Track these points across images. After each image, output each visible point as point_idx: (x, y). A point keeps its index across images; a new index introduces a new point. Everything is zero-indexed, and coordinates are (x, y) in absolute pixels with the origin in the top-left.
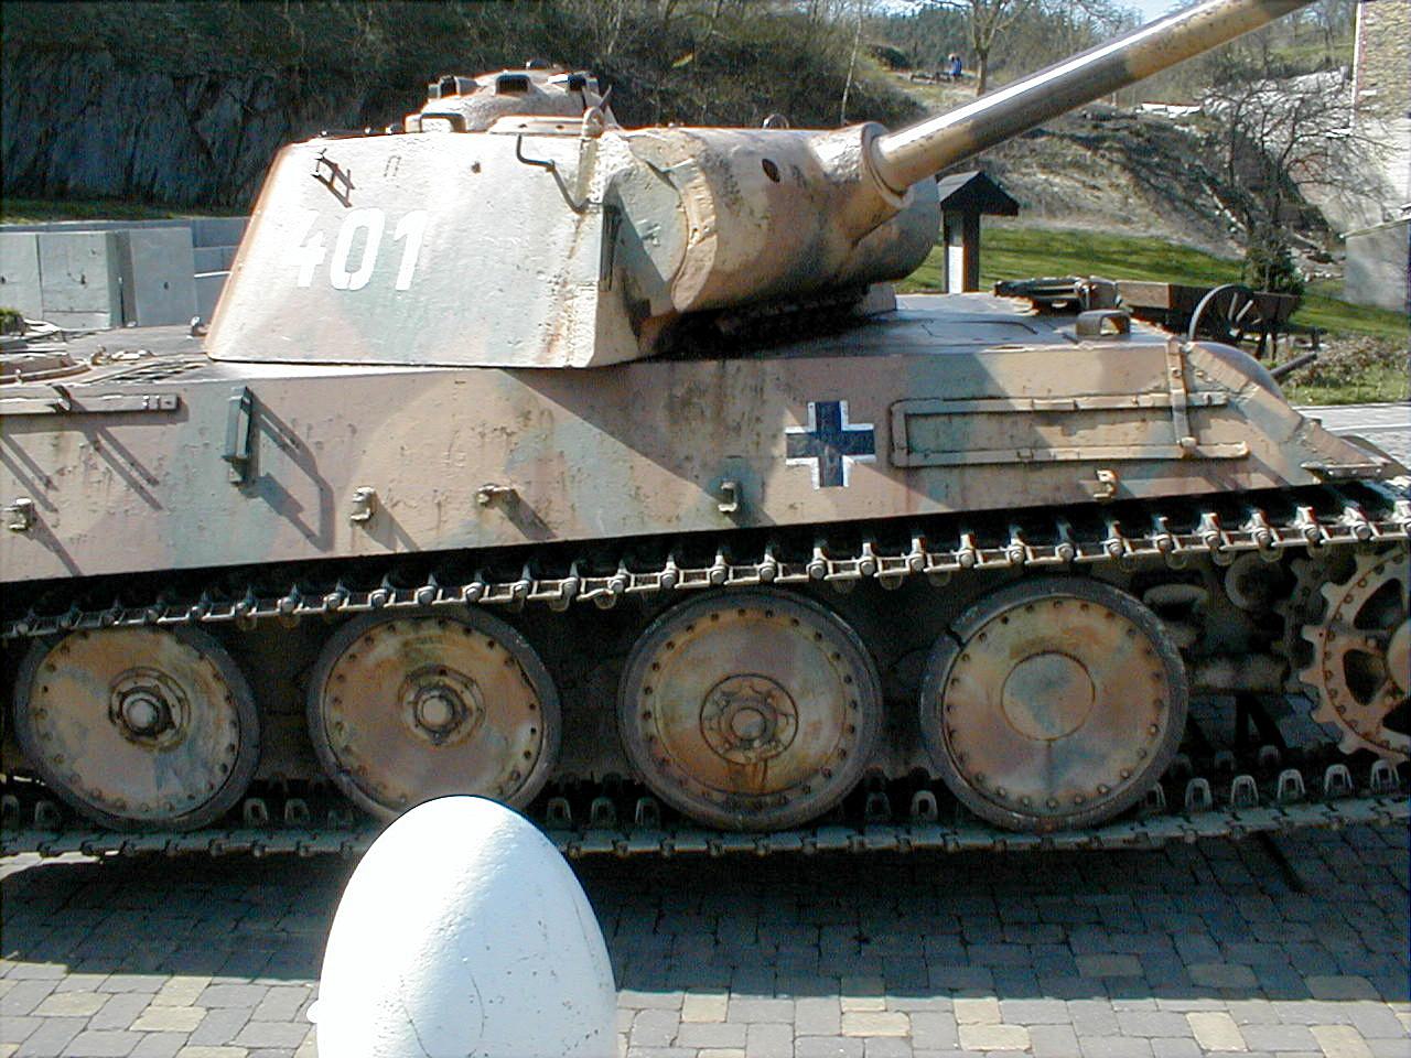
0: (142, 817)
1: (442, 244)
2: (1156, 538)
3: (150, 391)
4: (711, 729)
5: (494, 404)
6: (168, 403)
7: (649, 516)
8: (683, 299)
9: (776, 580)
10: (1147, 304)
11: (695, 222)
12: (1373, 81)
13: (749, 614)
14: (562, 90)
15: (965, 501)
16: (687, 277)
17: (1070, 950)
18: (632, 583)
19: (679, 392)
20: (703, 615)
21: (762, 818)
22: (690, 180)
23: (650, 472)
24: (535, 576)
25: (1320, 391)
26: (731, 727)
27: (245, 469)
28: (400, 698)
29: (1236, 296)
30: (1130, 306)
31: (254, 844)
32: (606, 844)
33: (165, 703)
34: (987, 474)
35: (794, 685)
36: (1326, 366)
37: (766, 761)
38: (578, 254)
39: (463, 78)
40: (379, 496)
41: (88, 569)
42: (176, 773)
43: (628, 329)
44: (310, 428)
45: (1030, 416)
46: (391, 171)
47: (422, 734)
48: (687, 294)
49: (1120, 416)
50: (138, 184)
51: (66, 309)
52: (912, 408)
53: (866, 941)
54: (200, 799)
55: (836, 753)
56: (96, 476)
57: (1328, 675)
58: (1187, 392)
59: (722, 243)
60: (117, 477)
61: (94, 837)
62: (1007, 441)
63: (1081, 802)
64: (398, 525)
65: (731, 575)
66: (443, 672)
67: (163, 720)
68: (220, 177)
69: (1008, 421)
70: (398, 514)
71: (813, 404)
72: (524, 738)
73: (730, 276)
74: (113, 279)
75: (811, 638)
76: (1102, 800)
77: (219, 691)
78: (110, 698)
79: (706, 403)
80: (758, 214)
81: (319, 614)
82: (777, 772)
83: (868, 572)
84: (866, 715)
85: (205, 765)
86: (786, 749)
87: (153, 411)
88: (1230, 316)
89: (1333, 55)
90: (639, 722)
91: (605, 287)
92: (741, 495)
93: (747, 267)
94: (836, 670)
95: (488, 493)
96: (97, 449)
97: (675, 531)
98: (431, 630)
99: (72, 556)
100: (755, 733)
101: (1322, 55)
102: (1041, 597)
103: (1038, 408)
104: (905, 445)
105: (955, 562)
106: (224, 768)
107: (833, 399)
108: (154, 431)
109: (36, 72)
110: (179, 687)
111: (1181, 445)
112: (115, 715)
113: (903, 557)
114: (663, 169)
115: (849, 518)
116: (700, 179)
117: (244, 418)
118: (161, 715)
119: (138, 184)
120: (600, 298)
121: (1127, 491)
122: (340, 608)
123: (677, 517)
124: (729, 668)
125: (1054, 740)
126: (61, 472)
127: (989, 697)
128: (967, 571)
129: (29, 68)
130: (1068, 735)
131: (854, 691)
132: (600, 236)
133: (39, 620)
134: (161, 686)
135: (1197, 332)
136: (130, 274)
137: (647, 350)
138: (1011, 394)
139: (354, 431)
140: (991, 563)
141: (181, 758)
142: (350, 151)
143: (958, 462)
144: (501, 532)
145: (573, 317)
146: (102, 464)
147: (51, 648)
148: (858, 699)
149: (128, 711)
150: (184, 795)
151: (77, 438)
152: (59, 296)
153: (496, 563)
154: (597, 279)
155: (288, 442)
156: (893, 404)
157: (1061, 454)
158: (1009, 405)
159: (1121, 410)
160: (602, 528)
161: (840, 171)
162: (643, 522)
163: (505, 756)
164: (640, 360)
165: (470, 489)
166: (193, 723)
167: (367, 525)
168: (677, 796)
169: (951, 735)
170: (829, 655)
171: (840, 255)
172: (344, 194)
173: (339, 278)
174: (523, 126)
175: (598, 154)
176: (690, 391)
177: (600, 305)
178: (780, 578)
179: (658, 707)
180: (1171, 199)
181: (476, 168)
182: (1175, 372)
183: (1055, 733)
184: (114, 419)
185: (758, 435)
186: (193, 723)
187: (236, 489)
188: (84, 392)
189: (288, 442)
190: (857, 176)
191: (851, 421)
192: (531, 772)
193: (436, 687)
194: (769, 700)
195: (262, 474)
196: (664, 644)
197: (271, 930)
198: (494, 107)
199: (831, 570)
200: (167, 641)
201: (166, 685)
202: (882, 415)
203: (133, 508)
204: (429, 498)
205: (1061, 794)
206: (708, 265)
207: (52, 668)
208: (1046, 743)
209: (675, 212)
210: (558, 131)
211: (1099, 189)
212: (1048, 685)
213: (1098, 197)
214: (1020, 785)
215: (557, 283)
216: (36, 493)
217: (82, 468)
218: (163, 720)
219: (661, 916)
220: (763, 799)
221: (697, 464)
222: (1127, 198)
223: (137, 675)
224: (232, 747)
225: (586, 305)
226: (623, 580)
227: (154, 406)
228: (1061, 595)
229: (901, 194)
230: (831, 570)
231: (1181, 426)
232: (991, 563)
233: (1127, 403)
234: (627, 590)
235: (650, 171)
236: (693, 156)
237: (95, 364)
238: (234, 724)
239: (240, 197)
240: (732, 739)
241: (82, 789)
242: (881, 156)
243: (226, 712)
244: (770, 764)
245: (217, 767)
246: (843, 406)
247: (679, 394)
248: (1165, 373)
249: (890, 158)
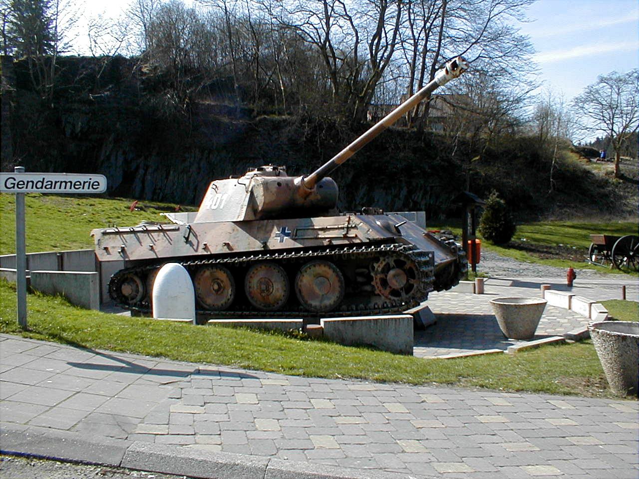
5: (229, 227)
14: (272, 170)
27: (187, 239)
35: (273, 281)
43: (253, 213)
47: (214, 292)
57: (377, 283)
70: (210, 247)
79: (264, 228)
92: (265, 245)
109: (238, 166)
116: (262, 186)
117: (188, 230)
124: (261, 277)
129: (236, 166)
146: (165, 239)
165: (222, 243)
233: (336, 227)
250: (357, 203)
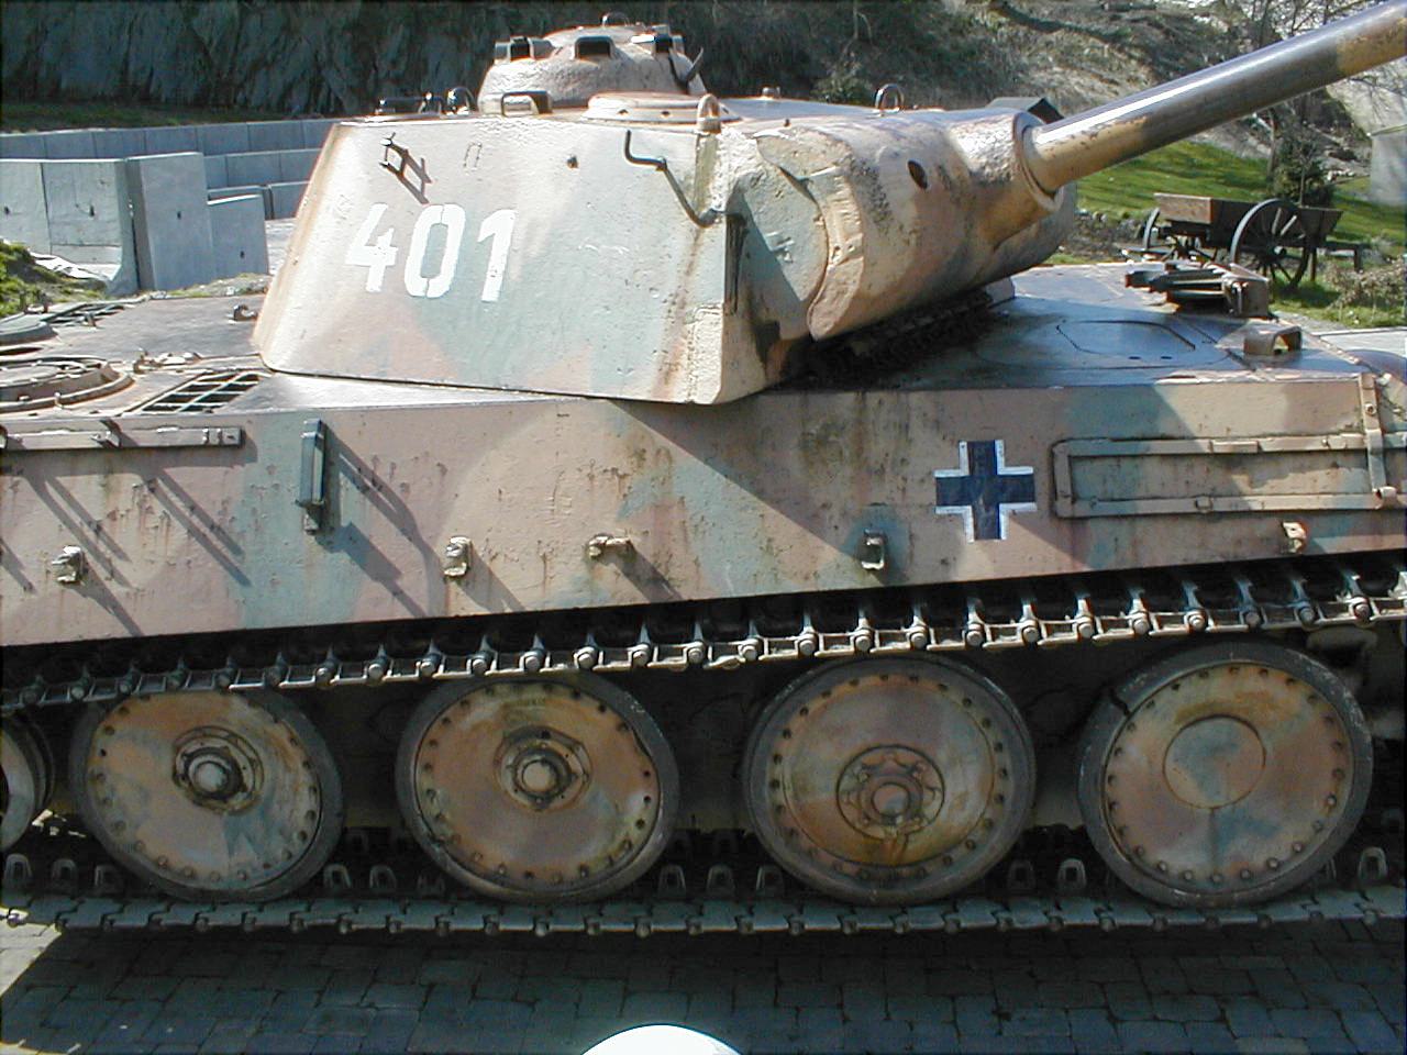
0: (213, 887)
1: (535, 250)
2: (1350, 600)
3: (208, 423)
4: (849, 803)
5: (603, 441)
6: (231, 437)
7: (784, 573)
8: (821, 324)
9: (929, 647)
10: (1187, 218)
11: (837, 239)
13: (892, 678)
14: (648, 53)
15: (1136, 555)
16: (825, 300)
17: (1228, 1029)
18: (766, 650)
19: (814, 429)
20: (841, 682)
21: (900, 892)
22: (834, 192)
23: (785, 529)
24: (655, 639)
25: (1365, 311)
26: (872, 802)
27: (322, 515)
28: (497, 762)
29: (1280, 210)
30: (1168, 220)
31: (339, 920)
32: (729, 922)
33: (235, 764)
34: (1161, 525)
35: (942, 757)
36: (1374, 284)
37: (907, 835)
38: (698, 271)
39: (536, 39)
40: (476, 548)
42: (250, 840)
43: (755, 357)
44: (393, 466)
45: (1207, 460)
46: (471, 159)
47: (521, 799)
48: (826, 320)
49: (1307, 460)
50: (134, 86)
51: (74, 242)
52: (1079, 449)
53: (1007, 1017)
54: (278, 868)
55: (981, 824)
56: (152, 521)
58: (1384, 431)
59: (869, 265)
60: (176, 523)
61: (161, 907)
62: (1182, 490)
63: (1247, 876)
64: (498, 581)
65: (877, 642)
66: (546, 734)
67: (234, 782)
68: (219, 75)
69: (1182, 465)
70: (498, 568)
71: (964, 444)
72: (636, 806)
73: (875, 300)
74: (123, 209)
75: (961, 703)
76: (1275, 876)
77: (297, 757)
78: (174, 760)
79: (845, 442)
80: (908, 229)
81: (411, 682)
82: (917, 845)
83: (1031, 639)
84: (1018, 787)
85: (281, 832)
86: (930, 823)
87: (215, 446)
88: (1274, 231)
90: (766, 791)
91: (731, 309)
93: (894, 287)
94: (986, 738)
95: (601, 546)
96: (152, 490)
97: (813, 589)
98: (535, 693)
99: (130, 612)
100: (899, 808)
102: (1215, 663)
103: (1216, 450)
104: (1069, 492)
105: (1127, 626)
106: (303, 835)
107: (988, 439)
108: (215, 474)
110: (251, 748)
111: (1379, 493)
112: (180, 777)
113: (1068, 620)
114: (800, 176)
115: (1008, 576)
117: (319, 455)
118: (232, 777)
119: (134, 86)
120: (726, 324)
121: (1317, 546)
122: (435, 676)
123: (815, 573)
124: (870, 739)
125: (1217, 808)
126: (112, 516)
127: (1150, 762)
128: (1142, 638)
130: (1234, 803)
131: (1005, 759)
132: (724, 250)
133: (96, 681)
134: (231, 747)
135: (1239, 250)
136: (142, 201)
137: (775, 377)
138: (1197, 435)
139: (443, 471)
140: (1167, 629)
141: (253, 822)
142: (414, 133)
143: (1129, 512)
144: (615, 589)
145: (694, 344)
146: (159, 508)
147: (108, 711)
148: (1009, 768)
149: (195, 774)
150: (258, 862)
151: (130, 480)
152: (67, 228)
153: (612, 625)
154: (722, 301)
155: (370, 484)
156: (1054, 445)
158: (1245, 502)
159: (1310, 452)
160: (731, 586)
161: (988, 170)
162: (777, 580)
163: (616, 822)
164: (766, 391)
166: (266, 785)
167: (463, 583)
168: (810, 871)
169: (1111, 807)
170: (979, 721)
171: (982, 255)
172: (418, 188)
173: (415, 284)
174: (623, 112)
175: (718, 152)
176: (826, 427)
177: (726, 333)
178: (933, 645)
179: (787, 777)
181: (573, 163)
182: (1371, 409)
183: (1219, 801)
184: (170, 457)
185: (905, 479)
186: (267, 785)
187: (313, 538)
188: (133, 424)
189: (370, 484)
190: (1008, 175)
191: (1008, 464)
192: (646, 841)
193: (539, 750)
194: (915, 774)
195: (344, 524)
196: (799, 709)
197: (357, 1005)
198: (573, 73)
199: (989, 637)
200: (236, 702)
201: (236, 746)
202: (1043, 456)
203: (196, 559)
204: (533, 551)
205: (1227, 868)
206: (852, 289)
207: (109, 730)
208: (1208, 812)
209: (812, 226)
210: (663, 118)
211: (1117, 84)
212: (1215, 751)
213: (1116, 93)
214: (1183, 858)
215: (674, 303)
216: (85, 541)
217: (136, 512)
218: (234, 782)
219: (779, 983)
220: (898, 870)
221: (835, 511)
223: (205, 735)
224: (311, 814)
225: (709, 330)
226: (756, 646)
227: (214, 441)
228: (1241, 660)
229: (1052, 195)
230: (989, 637)
231: (1376, 472)
232: (1167, 629)
233: (1316, 444)
234: (761, 658)
235: (783, 177)
236: (836, 164)
237: (137, 371)
238: (313, 789)
239: (240, 96)
240: (872, 815)
241: (146, 857)
242: (1035, 153)
243: (305, 778)
244: (912, 838)
245: (295, 835)
246: (999, 445)
247: (813, 431)
248: (1358, 410)
249: (1046, 155)
250: (382, 75)
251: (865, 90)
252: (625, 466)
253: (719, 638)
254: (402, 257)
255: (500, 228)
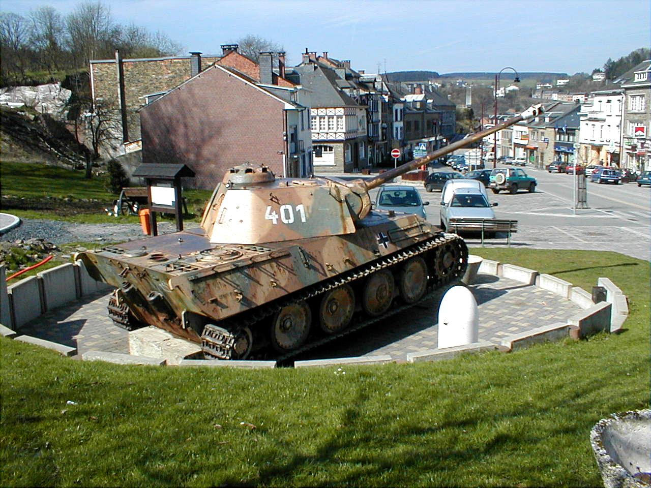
12: (101, 94)
41: (291, 291)
89: (54, 77)
101: (49, 76)
144: (350, 267)
157: (410, 236)
180: (29, 144)
222: (11, 145)
251: (49, 159)
252: (342, 246)
253: (363, 271)
254: (280, 216)
255: (300, 208)
